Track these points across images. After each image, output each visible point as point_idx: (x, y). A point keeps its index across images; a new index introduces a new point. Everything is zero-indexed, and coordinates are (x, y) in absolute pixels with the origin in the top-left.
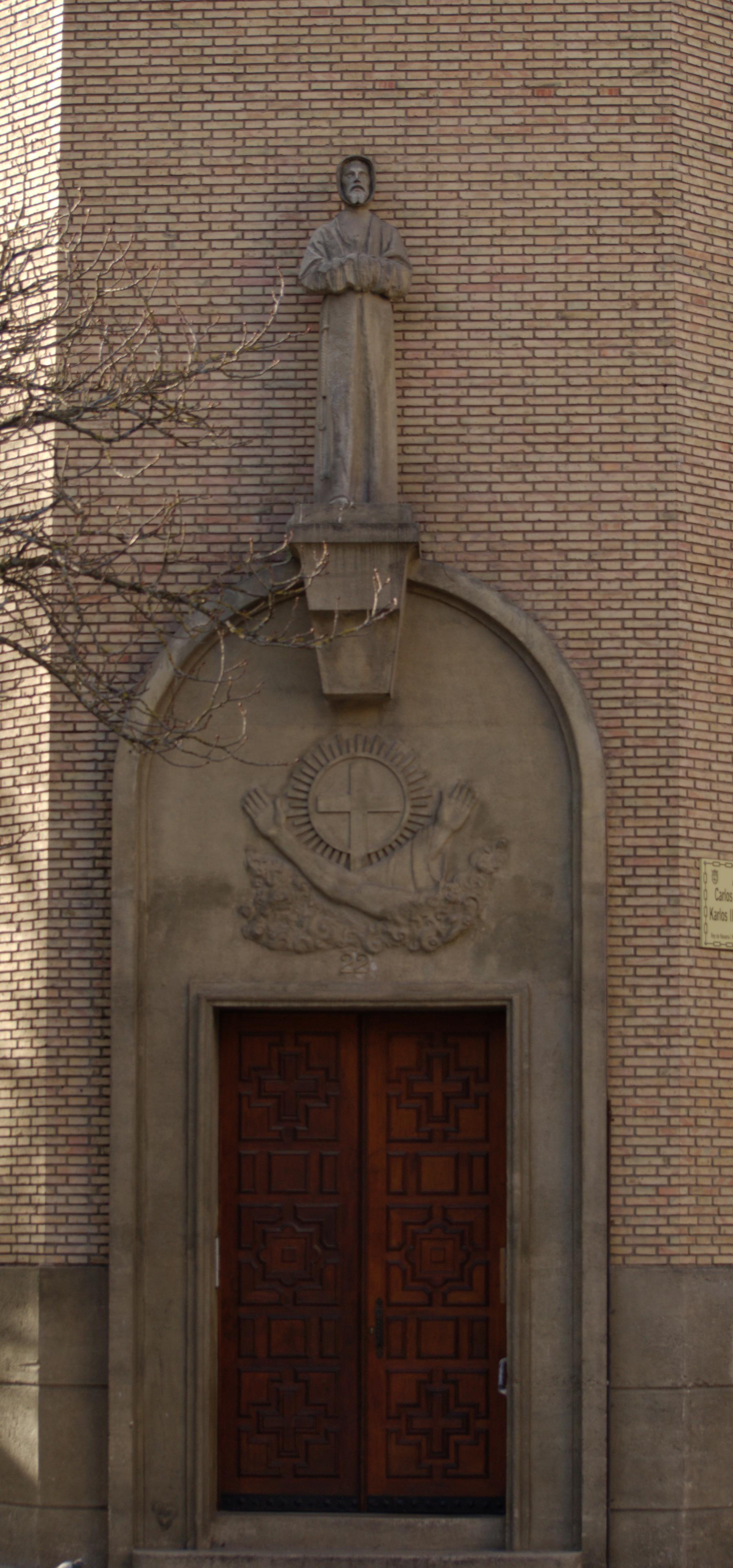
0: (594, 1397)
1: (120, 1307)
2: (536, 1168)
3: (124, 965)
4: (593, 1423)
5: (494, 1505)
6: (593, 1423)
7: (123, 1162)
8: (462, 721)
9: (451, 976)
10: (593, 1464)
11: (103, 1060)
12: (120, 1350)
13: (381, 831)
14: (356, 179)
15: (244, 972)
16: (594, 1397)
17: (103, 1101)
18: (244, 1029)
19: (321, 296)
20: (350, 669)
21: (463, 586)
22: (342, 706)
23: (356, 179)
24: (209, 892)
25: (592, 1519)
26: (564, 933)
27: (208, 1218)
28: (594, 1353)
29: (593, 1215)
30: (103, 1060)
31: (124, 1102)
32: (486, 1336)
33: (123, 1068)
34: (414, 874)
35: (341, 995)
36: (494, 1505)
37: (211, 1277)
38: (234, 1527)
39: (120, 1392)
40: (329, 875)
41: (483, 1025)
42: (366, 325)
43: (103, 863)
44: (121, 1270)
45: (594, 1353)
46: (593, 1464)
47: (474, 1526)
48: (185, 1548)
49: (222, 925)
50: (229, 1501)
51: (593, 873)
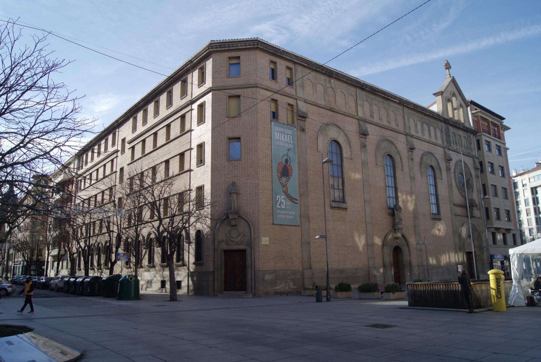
0: (253, 281)
1: (216, 274)
2: (248, 263)
3: (216, 247)
4: (253, 283)
5: (245, 290)
6: (253, 283)
7: (216, 263)
8: (242, 227)
9: (242, 247)
10: (253, 286)
11: (214, 255)
12: (216, 278)
13: (236, 236)
14: (233, 184)
15: (225, 247)
16: (253, 281)
17: (214, 258)
18: (226, 252)
19: (231, 193)
20: (233, 223)
21: (242, 216)
22: (233, 226)
23: (233, 184)
24: (223, 241)
25: (253, 291)
26: (250, 243)
27: (223, 267)
28: (253, 277)
29: (253, 266)
30: (214, 255)
31: (216, 258)
32: (245, 276)
33: (216, 255)
34: (239, 239)
35: (198, 94)
36: (245, 290)
37: (223, 272)
38: (225, 292)
39: (216, 281)
40: (232, 239)
41: (244, 251)
42: (234, 196)
43: (214, 239)
44: (216, 271)
45: (253, 277)
46: (253, 286)
47: (244, 292)
48: (489, 281)
49: (224, 243)
50: (225, 290)
51: (253, 238)
